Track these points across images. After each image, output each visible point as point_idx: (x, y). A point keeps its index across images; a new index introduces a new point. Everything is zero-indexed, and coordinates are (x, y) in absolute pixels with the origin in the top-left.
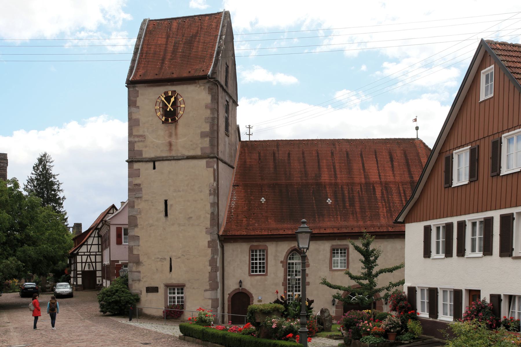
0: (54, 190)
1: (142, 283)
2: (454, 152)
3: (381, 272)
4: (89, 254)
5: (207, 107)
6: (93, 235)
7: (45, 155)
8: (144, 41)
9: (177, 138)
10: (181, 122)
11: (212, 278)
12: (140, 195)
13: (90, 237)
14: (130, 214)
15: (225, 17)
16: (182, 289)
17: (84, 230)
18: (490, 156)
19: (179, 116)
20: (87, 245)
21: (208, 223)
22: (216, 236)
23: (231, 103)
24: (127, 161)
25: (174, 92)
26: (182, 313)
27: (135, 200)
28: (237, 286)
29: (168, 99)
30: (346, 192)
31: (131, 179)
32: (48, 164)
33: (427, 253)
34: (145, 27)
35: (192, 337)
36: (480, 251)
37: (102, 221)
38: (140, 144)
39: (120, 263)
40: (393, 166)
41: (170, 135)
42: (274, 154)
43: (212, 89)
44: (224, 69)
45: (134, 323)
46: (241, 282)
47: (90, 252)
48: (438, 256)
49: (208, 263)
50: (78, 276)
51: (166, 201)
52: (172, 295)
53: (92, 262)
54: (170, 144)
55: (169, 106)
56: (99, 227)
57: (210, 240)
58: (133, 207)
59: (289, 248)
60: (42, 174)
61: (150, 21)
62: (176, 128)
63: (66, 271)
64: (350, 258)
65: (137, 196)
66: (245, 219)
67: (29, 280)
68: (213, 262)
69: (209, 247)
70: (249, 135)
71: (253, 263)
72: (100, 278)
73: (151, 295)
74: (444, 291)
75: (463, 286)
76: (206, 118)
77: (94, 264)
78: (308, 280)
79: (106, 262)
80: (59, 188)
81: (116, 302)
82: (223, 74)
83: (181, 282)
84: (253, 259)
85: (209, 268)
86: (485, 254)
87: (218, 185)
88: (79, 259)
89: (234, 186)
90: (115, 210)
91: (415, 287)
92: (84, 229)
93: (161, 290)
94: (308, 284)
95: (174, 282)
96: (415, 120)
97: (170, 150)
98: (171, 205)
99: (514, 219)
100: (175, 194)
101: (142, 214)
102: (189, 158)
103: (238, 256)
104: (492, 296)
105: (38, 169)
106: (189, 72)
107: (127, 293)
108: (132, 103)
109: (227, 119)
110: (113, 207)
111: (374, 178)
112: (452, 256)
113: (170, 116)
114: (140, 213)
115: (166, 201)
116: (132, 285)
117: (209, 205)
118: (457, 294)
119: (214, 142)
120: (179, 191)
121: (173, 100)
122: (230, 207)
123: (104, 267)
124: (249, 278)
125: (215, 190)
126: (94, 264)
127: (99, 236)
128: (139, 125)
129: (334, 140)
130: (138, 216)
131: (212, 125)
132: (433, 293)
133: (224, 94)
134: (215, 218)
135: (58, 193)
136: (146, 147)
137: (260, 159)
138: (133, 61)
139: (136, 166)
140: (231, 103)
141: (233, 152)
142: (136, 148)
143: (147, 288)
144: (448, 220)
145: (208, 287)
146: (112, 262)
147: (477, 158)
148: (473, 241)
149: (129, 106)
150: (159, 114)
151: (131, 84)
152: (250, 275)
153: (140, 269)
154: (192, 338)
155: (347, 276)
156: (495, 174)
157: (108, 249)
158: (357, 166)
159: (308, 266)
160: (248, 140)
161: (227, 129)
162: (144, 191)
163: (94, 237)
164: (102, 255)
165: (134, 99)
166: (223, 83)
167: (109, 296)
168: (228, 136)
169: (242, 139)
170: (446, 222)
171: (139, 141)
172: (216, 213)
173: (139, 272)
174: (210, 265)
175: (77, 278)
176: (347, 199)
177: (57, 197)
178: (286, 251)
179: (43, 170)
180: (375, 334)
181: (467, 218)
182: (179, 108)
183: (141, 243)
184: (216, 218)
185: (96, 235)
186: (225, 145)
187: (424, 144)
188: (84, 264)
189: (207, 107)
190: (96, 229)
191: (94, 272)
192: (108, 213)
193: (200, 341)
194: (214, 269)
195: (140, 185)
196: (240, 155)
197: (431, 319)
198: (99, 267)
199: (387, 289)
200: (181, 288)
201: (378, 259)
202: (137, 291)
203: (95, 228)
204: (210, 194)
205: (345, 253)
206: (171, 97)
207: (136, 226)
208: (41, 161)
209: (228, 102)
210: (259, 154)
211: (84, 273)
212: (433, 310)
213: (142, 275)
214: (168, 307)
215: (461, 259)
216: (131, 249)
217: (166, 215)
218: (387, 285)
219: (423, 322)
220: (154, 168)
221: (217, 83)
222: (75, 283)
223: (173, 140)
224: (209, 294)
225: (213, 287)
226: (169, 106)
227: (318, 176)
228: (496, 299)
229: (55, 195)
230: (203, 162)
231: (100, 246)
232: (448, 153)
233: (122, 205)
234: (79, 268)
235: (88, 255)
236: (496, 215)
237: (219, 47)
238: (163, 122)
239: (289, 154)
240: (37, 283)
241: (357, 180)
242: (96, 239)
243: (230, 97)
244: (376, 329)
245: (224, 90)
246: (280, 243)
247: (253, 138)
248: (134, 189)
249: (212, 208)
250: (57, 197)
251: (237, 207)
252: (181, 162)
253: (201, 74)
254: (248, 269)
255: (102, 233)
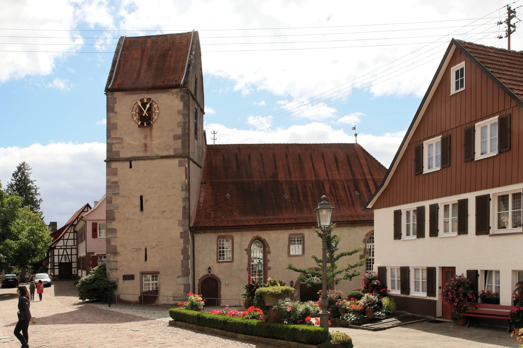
0: (32, 194)
1: (118, 272)
2: (424, 142)
3: (342, 255)
4: (65, 247)
5: (179, 112)
6: (69, 231)
7: (23, 164)
8: (121, 54)
9: (152, 141)
10: (155, 126)
11: (184, 265)
12: (117, 192)
13: (66, 232)
14: (108, 209)
15: (194, 36)
16: (156, 276)
17: (58, 228)
18: (463, 143)
19: (154, 120)
20: (64, 239)
21: (180, 215)
22: (188, 227)
23: (199, 111)
24: (105, 161)
25: (149, 99)
26: (156, 298)
27: (113, 196)
28: (206, 273)
29: (144, 105)
30: (300, 188)
31: (109, 177)
32: (26, 171)
33: (398, 235)
34: (122, 44)
35: (186, 322)
36: (413, 235)
37: (77, 218)
38: (118, 146)
39: (95, 254)
40: (338, 167)
41: (146, 138)
42: (236, 156)
43: (184, 97)
44: (194, 79)
45: (114, 309)
46: (209, 268)
47: (66, 246)
48: (408, 238)
49: (180, 252)
50: (55, 267)
51: (141, 197)
52: (147, 282)
53: (68, 255)
54: (146, 146)
55: (145, 112)
56: (75, 223)
57: (182, 231)
58: (111, 202)
59: (252, 237)
60: (21, 180)
61: (126, 38)
62: (151, 131)
63: (44, 264)
64: (305, 245)
65: (114, 192)
66: (212, 213)
67: (10, 271)
68: (184, 251)
69: (181, 237)
70: (214, 139)
71: (220, 252)
72: (76, 269)
73: (127, 282)
74: (415, 269)
75: (437, 263)
76: (179, 123)
77: (70, 256)
78: (269, 265)
79: (82, 254)
80: (36, 192)
81: (95, 290)
82: (193, 84)
83: (156, 270)
84: (220, 248)
85: (182, 257)
86: (459, 233)
87: (189, 182)
88: (56, 252)
89: (202, 183)
90: (89, 208)
91: (385, 267)
92: (59, 227)
93: (137, 277)
94: (269, 261)
95: (149, 270)
96: (354, 128)
97: (146, 150)
98: (147, 200)
99: (490, 199)
100: (149, 190)
101: (120, 209)
102: (162, 157)
103: (206, 244)
104: (469, 272)
105: (17, 176)
106: (163, 82)
107: (105, 281)
108: (110, 109)
109: (196, 124)
110: (88, 206)
111: (323, 176)
112: (424, 237)
113: (146, 120)
114: (117, 208)
115: (141, 197)
116: (109, 273)
117: (181, 200)
118: (431, 271)
119: (186, 144)
120: (154, 188)
121: (148, 106)
122: (199, 202)
123: (79, 260)
124: (217, 264)
125: (186, 186)
126: (70, 256)
127: (75, 232)
128: (117, 129)
129: (287, 144)
130: (115, 211)
131: (184, 129)
132: (405, 272)
133: (194, 102)
134: (186, 212)
135: (36, 196)
136: (123, 148)
137: (224, 160)
138: (112, 72)
139: (114, 165)
140: (199, 111)
141: (200, 153)
142: (114, 149)
143: (123, 276)
144: (420, 204)
145: (180, 274)
146: (88, 254)
147: (509, 127)
148: (446, 223)
149: (107, 111)
150: (135, 118)
151: (108, 91)
152: (218, 262)
153: (118, 258)
154: (184, 324)
155: (314, 259)
156: (419, 172)
157: (84, 242)
158: (307, 166)
159: (269, 253)
160: (213, 144)
161: (196, 133)
162: (121, 187)
163: (70, 232)
164: (77, 248)
165: (113, 105)
166: (193, 93)
167: (88, 285)
168: (197, 140)
169: (208, 143)
170: (418, 206)
171: (116, 143)
172: (187, 207)
173: (117, 262)
174: (182, 254)
175: (54, 269)
176: (301, 195)
177: (35, 200)
178: (250, 240)
179: (22, 177)
180: (355, 312)
181: (441, 202)
182: (154, 114)
183: (118, 234)
184: (187, 211)
185: (72, 231)
186: (194, 147)
187: (362, 148)
188: (60, 257)
189: (179, 112)
190: (72, 225)
191: (70, 263)
192: (83, 211)
193: (194, 326)
194: (186, 257)
195: (117, 182)
196: (206, 156)
197: (403, 296)
198: (74, 259)
199: (346, 270)
200: (155, 275)
201: (339, 244)
202: (114, 279)
203: (71, 225)
204: (182, 190)
205: (301, 241)
206: (147, 103)
207: (114, 219)
208: (20, 169)
209: (196, 110)
210: (224, 156)
211: (60, 264)
212: (405, 286)
213: (119, 264)
214: (144, 293)
215: (434, 239)
216: (108, 241)
217: (142, 209)
218: (347, 267)
219: (395, 298)
220: (131, 167)
221: (188, 92)
222: (52, 274)
223: (148, 142)
224: (181, 280)
225: (185, 274)
226: (145, 112)
227: (275, 175)
228: (473, 274)
229: (32, 199)
230: (176, 161)
231: (75, 240)
232: (418, 143)
233: (95, 205)
234: (56, 260)
235: (64, 249)
236: (471, 197)
237: (189, 61)
238: (139, 126)
239: (249, 156)
240: (17, 275)
241: (308, 178)
242: (72, 234)
243: (199, 105)
244: (354, 307)
245: (194, 99)
246: (244, 233)
247: (217, 143)
248: (112, 186)
249: (184, 203)
250: (35, 200)
251: (205, 202)
252: (157, 162)
253: (174, 83)
254: (216, 256)
255: (78, 228)
